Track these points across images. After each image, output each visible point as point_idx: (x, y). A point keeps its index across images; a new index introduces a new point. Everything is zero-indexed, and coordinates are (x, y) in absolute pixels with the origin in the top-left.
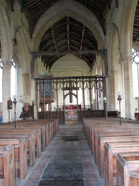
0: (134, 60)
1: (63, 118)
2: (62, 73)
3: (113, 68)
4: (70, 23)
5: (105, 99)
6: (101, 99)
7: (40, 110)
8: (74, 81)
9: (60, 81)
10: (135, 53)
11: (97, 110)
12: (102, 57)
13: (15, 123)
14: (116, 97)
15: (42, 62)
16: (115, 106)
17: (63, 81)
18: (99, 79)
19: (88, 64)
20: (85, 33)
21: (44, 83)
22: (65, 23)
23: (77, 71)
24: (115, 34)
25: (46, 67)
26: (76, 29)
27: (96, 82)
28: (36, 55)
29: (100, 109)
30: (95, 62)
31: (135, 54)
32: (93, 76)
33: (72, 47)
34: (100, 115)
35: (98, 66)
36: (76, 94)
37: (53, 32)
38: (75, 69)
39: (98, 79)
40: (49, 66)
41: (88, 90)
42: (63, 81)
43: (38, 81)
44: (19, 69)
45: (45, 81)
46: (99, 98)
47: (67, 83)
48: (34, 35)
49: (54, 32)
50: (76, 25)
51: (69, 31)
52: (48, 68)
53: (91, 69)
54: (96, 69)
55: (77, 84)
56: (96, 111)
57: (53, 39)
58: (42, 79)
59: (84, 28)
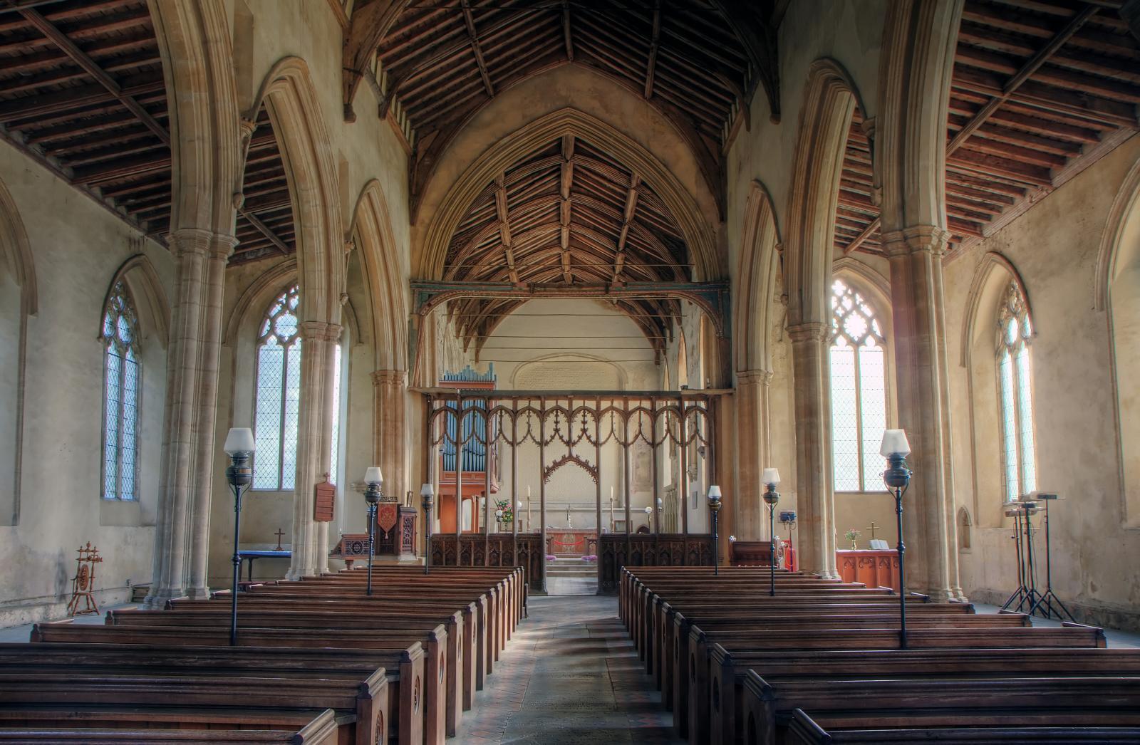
0: (841, 330)
1: (536, 562)
2: (531, 365)
3: (753, 360)
4: (576, 162)
5: (716, 491)
6: (702, 489)
7: (436, 528)
8: (590, 411)
9: (529, 409)
10: (845, 298)
11: (680, 531)
12: (708, 313)
13: (772, 574)
14: (763, 490)
15: (449, 321)
16: (755, 518)
17: (543, 406)
18: (693, 403)
19: (647, 331)
20: (638, 205)
21: (459, 413)
22: (555, 160)
23: (597, 359)
24: (764, 225)
25: (465, 339)
26: (601, 185)
27: (680, 413)
28: (430, 296)
29: (691, 531)
30: (676, 328)
31: (848, 303)
32: (667, 389)
33: (580, 255)
34: (693, 556)
35: (689, 346)
36: (592, 463)
37: (502, 195)
38: (590, 352)
39: (686, 404)
40: (476, 334)
41: (646, 449)
42: (543, 406)
43: (437, 405)
44: (357, 350)
45: (467, 404)
46: (691, 480)
47: (557, 416)
48: (425, 213)
49: (509, 197)
50: (600, 169)
51: (571, 191)
52: (472, 343)
53: (658, 354)
54: (679, 355)
55: (570, 421)
56: (673, 538)
57: (502, 222)
58: (452, 396)
59: (634, 184)
